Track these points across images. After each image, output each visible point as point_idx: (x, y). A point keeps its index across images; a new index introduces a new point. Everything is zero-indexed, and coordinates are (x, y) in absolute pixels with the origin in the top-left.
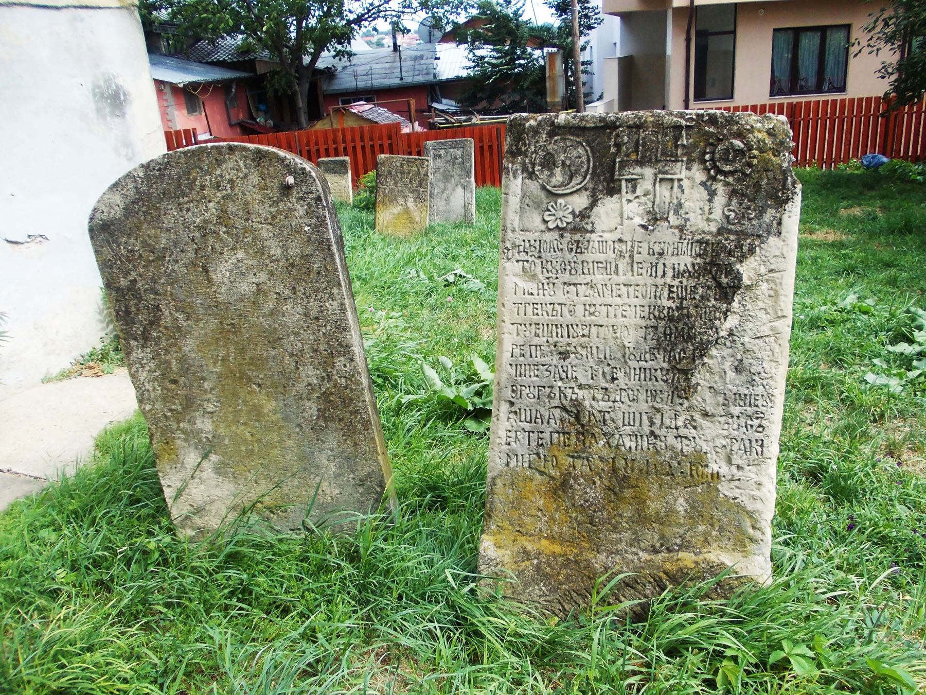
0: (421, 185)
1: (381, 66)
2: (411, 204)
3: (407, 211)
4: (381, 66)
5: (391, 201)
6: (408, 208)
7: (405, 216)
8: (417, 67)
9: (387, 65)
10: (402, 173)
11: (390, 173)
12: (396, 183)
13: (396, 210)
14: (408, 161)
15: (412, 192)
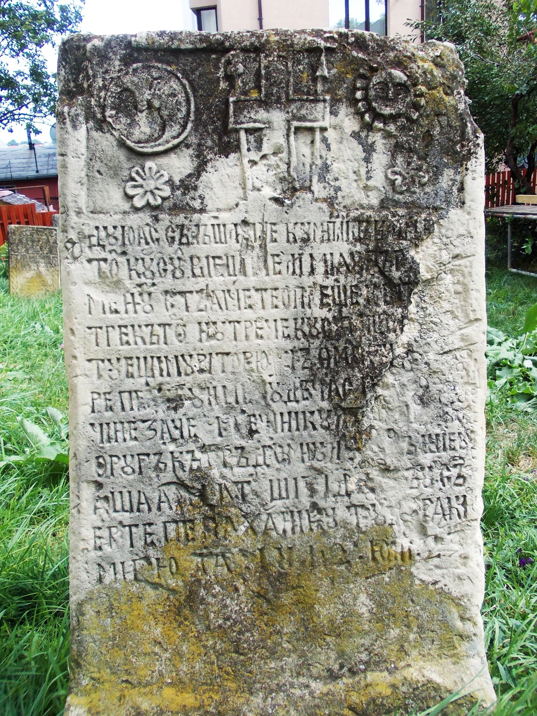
0: (51, 252)
1: (18, 161)
2: (42, 268)
3: (39, 275)
4: (18, 161)
5: (23, 266)
6: (40, 272)
7: (38, 280)
8: (51, 162)
9: (24, 161)
10: (33, 241)
11: (20, 241)
12: (27, 251)
13: (29, 274)
14: (38, 231)
15: (44, 258)
